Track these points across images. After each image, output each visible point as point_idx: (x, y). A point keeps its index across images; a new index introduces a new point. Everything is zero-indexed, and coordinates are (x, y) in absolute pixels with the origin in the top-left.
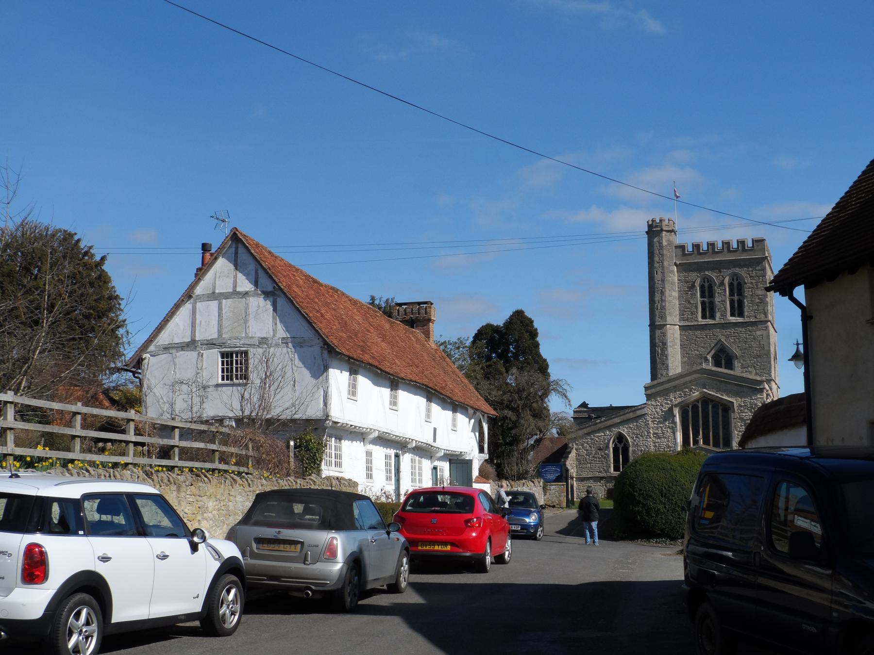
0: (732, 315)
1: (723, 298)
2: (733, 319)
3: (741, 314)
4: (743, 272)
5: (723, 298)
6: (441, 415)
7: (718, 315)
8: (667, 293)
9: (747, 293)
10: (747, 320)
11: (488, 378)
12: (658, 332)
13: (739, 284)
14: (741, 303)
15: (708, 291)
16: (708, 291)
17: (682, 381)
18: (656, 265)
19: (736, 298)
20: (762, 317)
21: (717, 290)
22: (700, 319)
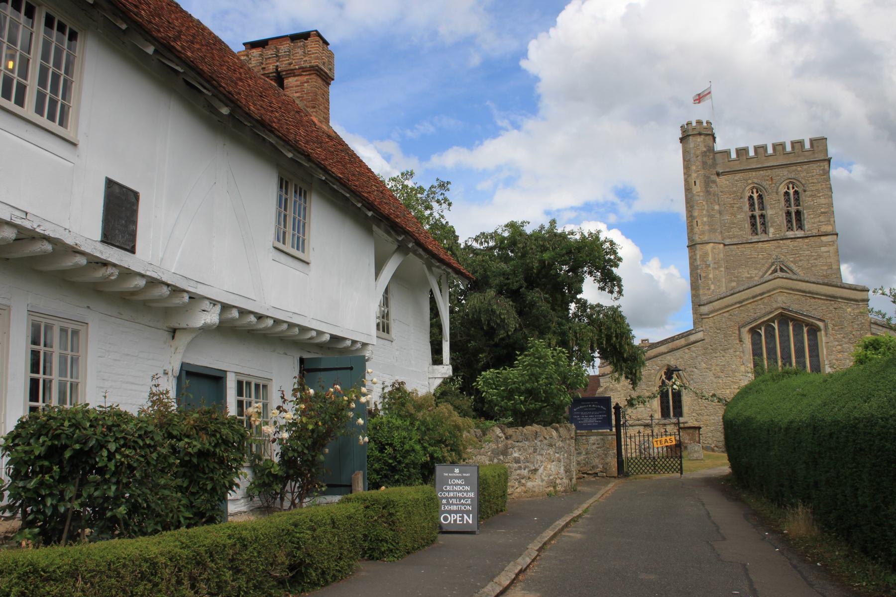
0: (790, 228)
1: (775, 212)
2: (790, 234)
3: (800, 227)
5: (775, 212)
7: (771, 230)
10: (784, 172)
14: (798, 213)
15: (757, 201)
19: (757, 213)
20: (828, 229)
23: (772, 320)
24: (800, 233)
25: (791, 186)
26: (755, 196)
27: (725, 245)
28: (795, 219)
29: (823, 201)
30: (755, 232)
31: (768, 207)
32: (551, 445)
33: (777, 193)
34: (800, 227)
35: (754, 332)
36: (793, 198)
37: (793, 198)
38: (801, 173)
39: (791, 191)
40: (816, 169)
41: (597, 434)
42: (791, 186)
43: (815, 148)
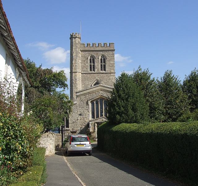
0: (102, 70)
1: (98, 65)
2: (101, 72)
3: (105, 70)
4: (106, 54)
5: (98, 65)
6: (22, 107)
7: (96, 70)
8: (78, 61)
9: (107, 62)
10: (107, 72)
11: (192, 112)
12: (74, 74)
13: (93, 59)
14: (104, 66)
15: (93, 60)
16: (93, 60)
17: (82, 93)
18: (74, 50)
19: (92, 64)
20: (112, 71)
21: (96, 60)
22: (89, 71)
23: (98, 99)
24: (104, 72)
25: (103, 57)
26: (92, 59)
27: (82, 73)
28: (104, 67)
29: (112, 62)
30: (91, 70)
31: (96, 62)
32: (51, 139)
33: (98, 58)
34: (105, 70)
35: (92, 102)
36: (104, 60)
37: (104, 60)
38: (106, 54)
39: (103, 59)
40: (111, 53)
41: (19, 92)
42: (103, 57)
43: (111, 46)
